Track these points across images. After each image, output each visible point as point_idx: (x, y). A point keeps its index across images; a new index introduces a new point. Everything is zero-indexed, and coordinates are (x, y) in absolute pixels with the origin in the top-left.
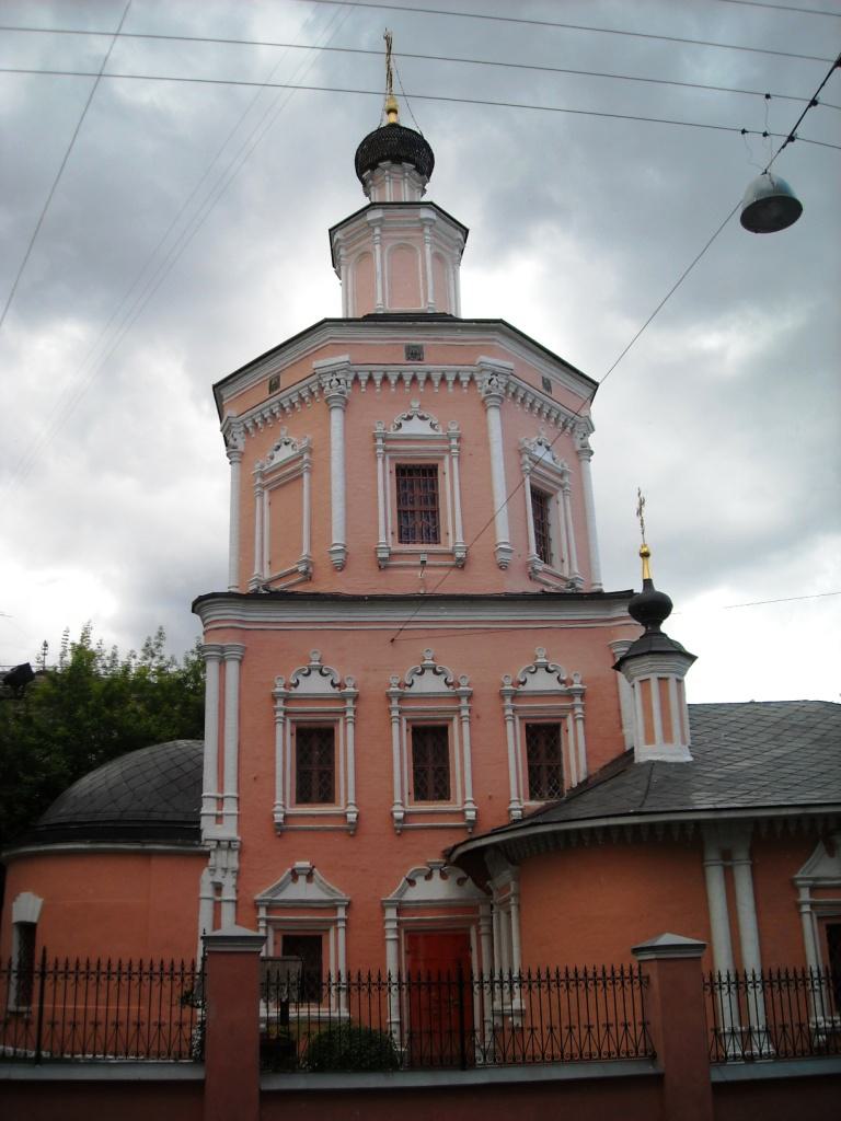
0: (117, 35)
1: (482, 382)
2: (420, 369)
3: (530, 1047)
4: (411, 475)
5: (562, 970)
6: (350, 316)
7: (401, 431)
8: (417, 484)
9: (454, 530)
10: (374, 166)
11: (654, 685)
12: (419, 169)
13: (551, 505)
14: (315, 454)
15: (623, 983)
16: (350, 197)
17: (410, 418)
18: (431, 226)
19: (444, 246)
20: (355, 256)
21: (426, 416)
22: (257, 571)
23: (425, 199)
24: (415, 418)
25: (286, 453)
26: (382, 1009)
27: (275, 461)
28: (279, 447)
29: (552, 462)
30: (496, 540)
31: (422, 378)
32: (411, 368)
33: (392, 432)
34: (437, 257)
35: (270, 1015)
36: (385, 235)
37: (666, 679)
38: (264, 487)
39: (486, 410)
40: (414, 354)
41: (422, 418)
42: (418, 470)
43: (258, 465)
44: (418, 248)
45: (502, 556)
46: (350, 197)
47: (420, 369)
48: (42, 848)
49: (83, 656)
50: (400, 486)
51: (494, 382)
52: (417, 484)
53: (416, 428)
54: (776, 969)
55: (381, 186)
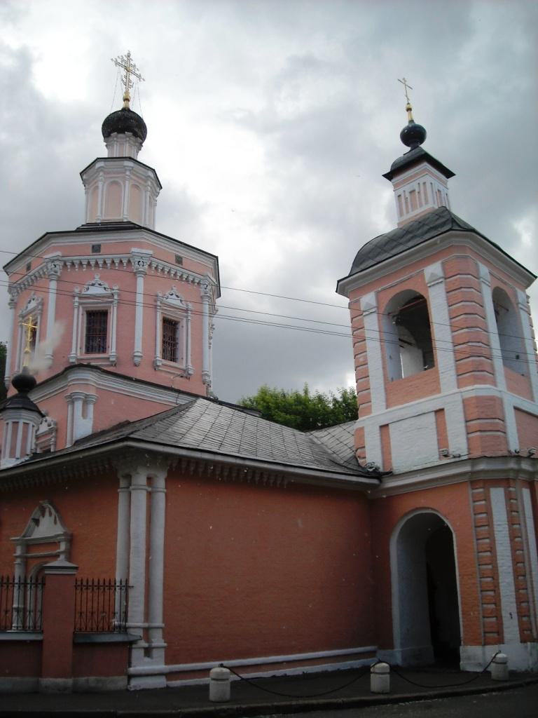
2: (99, 258)
3: (90, 624)
5: (96, 581)
8: (97, 321)
10: (121, 131)
11: (21, 426)
12: (135, 135)
13: (180, 326)
14: (43, 304)
15: (82, 589)
16: (100, 149)
18: (130, 170)
21: (94, 282)
22: (73, 352)
25: (33, 305)
27: (89, 292)
28: (30, 301)
30: (134, 349)
31: (101, 263)
32: (93, 258)
33: (83, 293)
35: (20, 606)
37: (28, 424)
38: (80, 304)
39: (136, 279)
42: (97, 313)
43: (21, 311)
44: (122, 183)
45: (137, 360)
46: (100, 149)
47: (99, 258)
49: (284, 396)
50: (89, 322)
51: (141, 263)
52: (97, 321)
54: (108, 580)
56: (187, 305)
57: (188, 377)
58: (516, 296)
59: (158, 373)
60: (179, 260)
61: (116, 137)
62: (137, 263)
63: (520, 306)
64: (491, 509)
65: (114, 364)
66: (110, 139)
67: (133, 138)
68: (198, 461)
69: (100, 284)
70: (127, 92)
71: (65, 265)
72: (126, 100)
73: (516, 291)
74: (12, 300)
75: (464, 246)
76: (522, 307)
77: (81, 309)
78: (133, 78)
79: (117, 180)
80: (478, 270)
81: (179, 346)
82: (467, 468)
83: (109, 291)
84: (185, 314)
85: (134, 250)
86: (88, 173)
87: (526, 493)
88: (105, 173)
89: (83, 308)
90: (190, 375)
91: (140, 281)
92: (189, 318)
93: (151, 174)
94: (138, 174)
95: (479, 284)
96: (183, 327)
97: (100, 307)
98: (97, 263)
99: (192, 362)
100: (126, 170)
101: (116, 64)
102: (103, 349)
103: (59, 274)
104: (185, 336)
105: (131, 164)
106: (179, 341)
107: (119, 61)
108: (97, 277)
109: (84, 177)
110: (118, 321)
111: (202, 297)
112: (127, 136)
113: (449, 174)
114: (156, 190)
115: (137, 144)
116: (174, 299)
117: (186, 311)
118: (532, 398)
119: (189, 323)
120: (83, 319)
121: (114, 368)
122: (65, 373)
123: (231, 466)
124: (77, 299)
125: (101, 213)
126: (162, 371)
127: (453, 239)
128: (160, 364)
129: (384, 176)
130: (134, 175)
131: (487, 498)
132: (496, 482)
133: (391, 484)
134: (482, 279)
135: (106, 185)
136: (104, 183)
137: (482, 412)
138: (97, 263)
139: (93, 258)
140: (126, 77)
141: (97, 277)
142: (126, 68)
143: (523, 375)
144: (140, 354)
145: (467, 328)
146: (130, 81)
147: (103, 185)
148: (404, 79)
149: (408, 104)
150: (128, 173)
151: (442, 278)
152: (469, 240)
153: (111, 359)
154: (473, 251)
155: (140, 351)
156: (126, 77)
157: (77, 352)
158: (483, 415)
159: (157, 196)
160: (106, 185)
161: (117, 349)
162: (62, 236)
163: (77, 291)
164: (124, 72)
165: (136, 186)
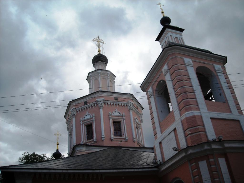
1: (129, 106)
7: (114, 114)
8: (89, 127)
9: (126, 134)
10: (97, 62)
12: (102, 61)
16: (92, 68)
17: (86, 115)
19: (95, 77)
21: (86, 115)
22: (82, 141)
24: (116, 112)
26: (212, 161)
27: (85, 118)
29: (120, 115)
33: (112, 114)
34: (110, 81)
38: (83, 123)
39: (100, 109)
41: (118, 112)
46: (92, 68)
52: (89, 127)
56: (123, 114)
57: (126, 141)
58: (214, 68)
59: (113, 142)
60: (116, 99)
61: (96, 64)
63: (217, 71)
64: (200, 173)
65: (95, 142)
66: (95, 65)
67: (102, 63)
68: (40, 174)
69: (88, 115)
70: (99, 49)
71: (77, 111)
72: (99, 51)
73: (214, 65)
74: (68, 128)
75: (175, 53)
76: (218, 71)
78: (101, 44)
79: (96, 78)
80: (184, 61)
81: (122, 130)
82: (183, 155)
83: (92, 116)
84: (122, 118)
85: (97, 99)
87: (222, 162)
88: (92, 77)
89: (84, 124)
90: (127, 140)
91: (101, 110)
92: (124, 119)
94: (104, 74)
95: (186, 67)
97: (89, 123)
99: (127, 135)
100: (99, 74)
101: (94, 41)
102: (92, 138)
103: (75, 115)
104: (124, 127)
105: (100, 71)
106: (122, 129)
107: (95, 40)
110: (95, 126)
111: (129, 110)
112: (99, 63)
113: (182, 30)
115: (104, 64)
116: (117, 114)
118: (231, 112)
119: (124, 121)
120: (85, 128)
121: (96, 144)
123: (45, 174)
124: (82, 122)
126: (114, 141)
127: (168, 52)
128: (113, 138)
130: (103, 75)
131: (198, 168)
132: (201, 159)
133: (163, 168)
134: (186, 65)
135: (93, 80)
136: (93, 80)
137: (190, 125)
140: (98, 44)
141: (87, 112)
142: (97, 41)
143: (224, 102)
144: (104, 136)
145: (179, 87)
146: (100, 45)
147: (92, 81)
148: (159, 3)
149: (162, 11)
150: (100, 74)
151: (168, 70)
152: (176, 50)
153: (94, 141)
154: (180, 54)
155: (104, 135)
156: (98, 44)
157: (84, 140)
158: (193, 125)
160: (93, 80)
161: (96, 136)
162: (75, 101)
163: (81, 119)
164: (97, 43)
165: (104, 78)
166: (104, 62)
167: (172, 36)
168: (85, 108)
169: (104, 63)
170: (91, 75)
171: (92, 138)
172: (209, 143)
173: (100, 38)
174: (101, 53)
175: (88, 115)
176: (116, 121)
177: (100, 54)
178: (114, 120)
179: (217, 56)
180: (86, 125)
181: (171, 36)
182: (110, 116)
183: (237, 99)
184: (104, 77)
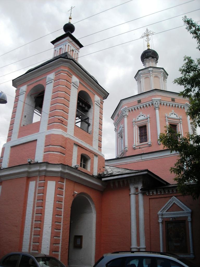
0: (24, 103)
4: (174, 126)
6: (140, 93)
7: (138, 119)
8: (143, 129)
10: (147, 57)
12: (153, 57)
13: (177, 126)
16: (141, 66)
20: (144, 77)
23: (158, 66)
27: (138, 119)
28: (140, 116)
29: (176, 117)
32: (138, 106)
36: (153, 73)
39: (155, 110)
40: (173, 100)
46: (141, 66)
47: (141, 105)
48: (191, 241)
51: (157, 103)
52: (143, 129)
53: (173, 116)
55: (147, 64)
60: (173, 100)
62: (155, 103)
67: (148, 59)
69: (142, 115)
70: (148, 43)
71: (129, 111)
72: (148, 46)
77: (136, 126)
79: (157, 75)
86: (137, 76)
89: (137, 126)
91: (157, 111)
93: (162, 70)
96: (179, 126)
98: (138, 108)
108: (173, 111)
109: (136, 78)
114: (166, 76)
116: (141, 118)
117: (179, 120)
120: (137, 131)
122: (42, 164)
125: (143, 90)
129: (51, 42)
138: (138, 108)
139: (138, 106)
141: (141, 113)
151: (25, 91)
153: (149, 144)
159: (167, 78)
163: (134, 120)
165: (156, 76)
166: (149, 58)
167: (70, 47)
168: (139, 107)
169: (150, 59)
170: (141, 73)
171: (146, 141)
172: (70, 168)
173: (149, 30)
174: (150, 48)
175: (142, 115)
176: (142, 126)
177: (149, 49)
178: (139, 126)
179: (87, 76)
180: (138, 127)
181: (69, 45)
182: (167, 118)
183: (102, 125)
184: (157, 75)
